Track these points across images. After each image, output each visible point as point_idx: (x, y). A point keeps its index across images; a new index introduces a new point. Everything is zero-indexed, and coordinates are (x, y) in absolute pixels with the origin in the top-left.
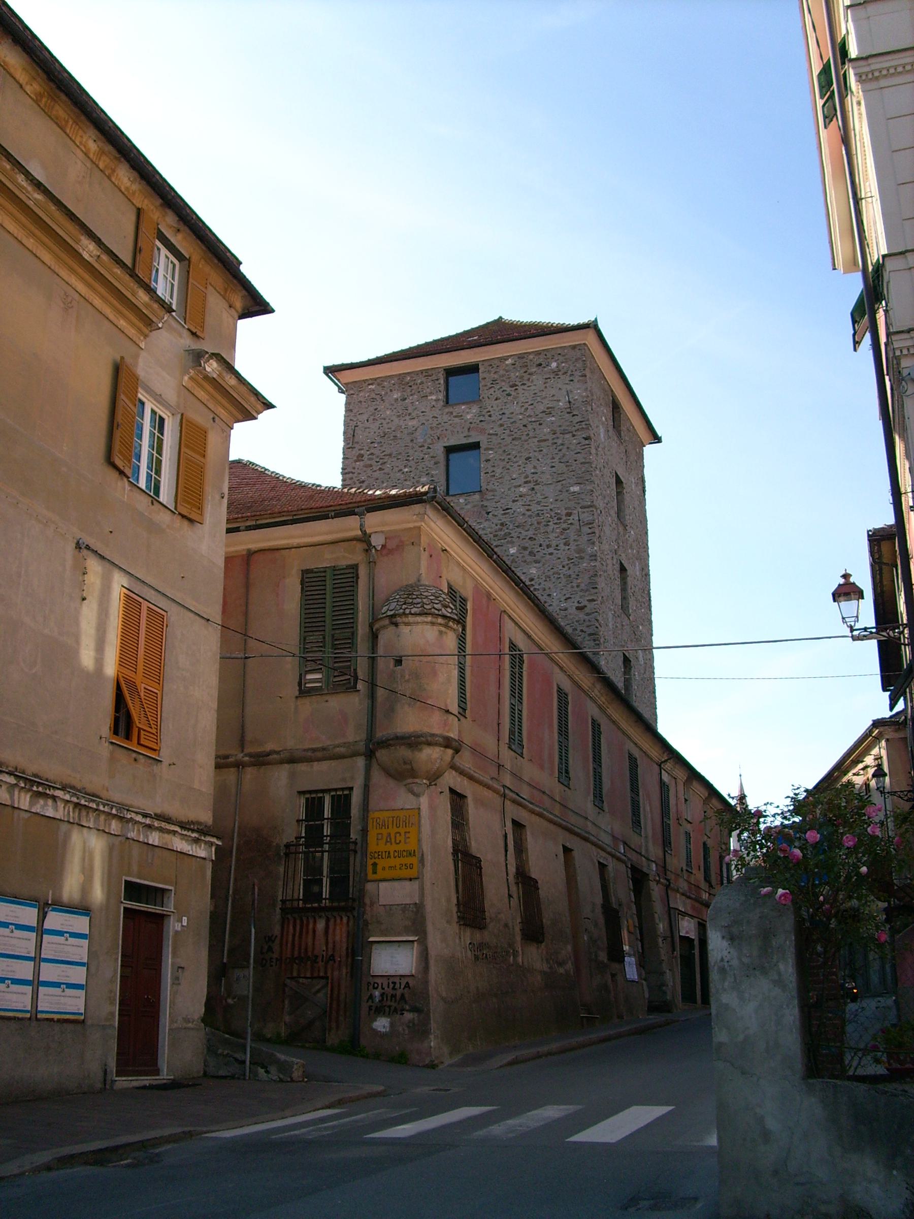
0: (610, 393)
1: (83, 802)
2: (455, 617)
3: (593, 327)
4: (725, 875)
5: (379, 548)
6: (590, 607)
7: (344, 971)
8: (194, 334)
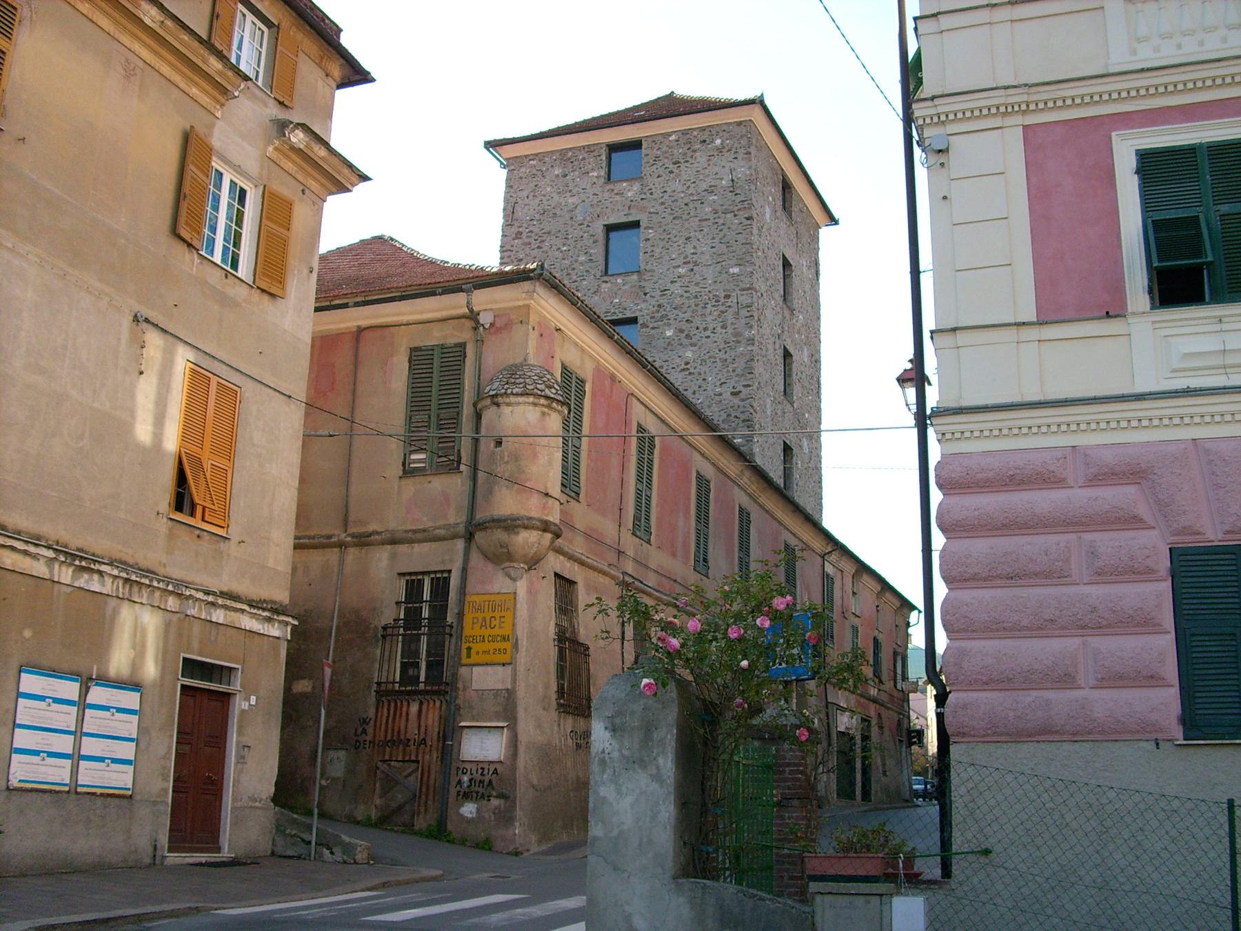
0: (780, 172)
1: (133, 578)
2: (560, 398)
3: (759, 102)
4: (899, 671)
5: (487, 326)
6: (745, 391)
7: (435, 756)
8: (281, 103)
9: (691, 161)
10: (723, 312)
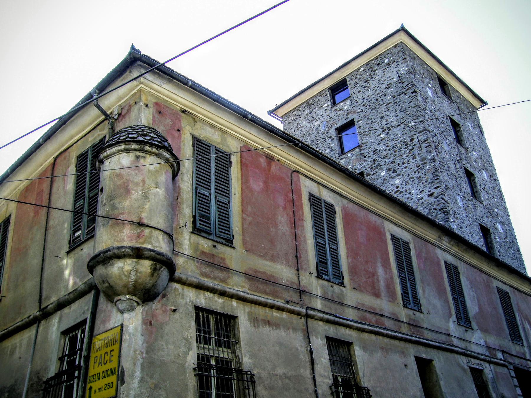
9: (374, 76)
10: (411, 150)
